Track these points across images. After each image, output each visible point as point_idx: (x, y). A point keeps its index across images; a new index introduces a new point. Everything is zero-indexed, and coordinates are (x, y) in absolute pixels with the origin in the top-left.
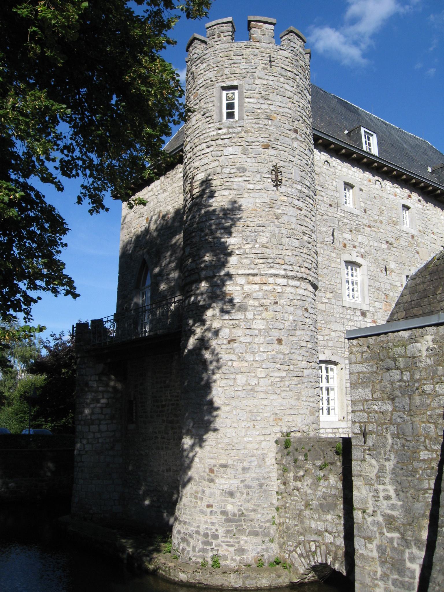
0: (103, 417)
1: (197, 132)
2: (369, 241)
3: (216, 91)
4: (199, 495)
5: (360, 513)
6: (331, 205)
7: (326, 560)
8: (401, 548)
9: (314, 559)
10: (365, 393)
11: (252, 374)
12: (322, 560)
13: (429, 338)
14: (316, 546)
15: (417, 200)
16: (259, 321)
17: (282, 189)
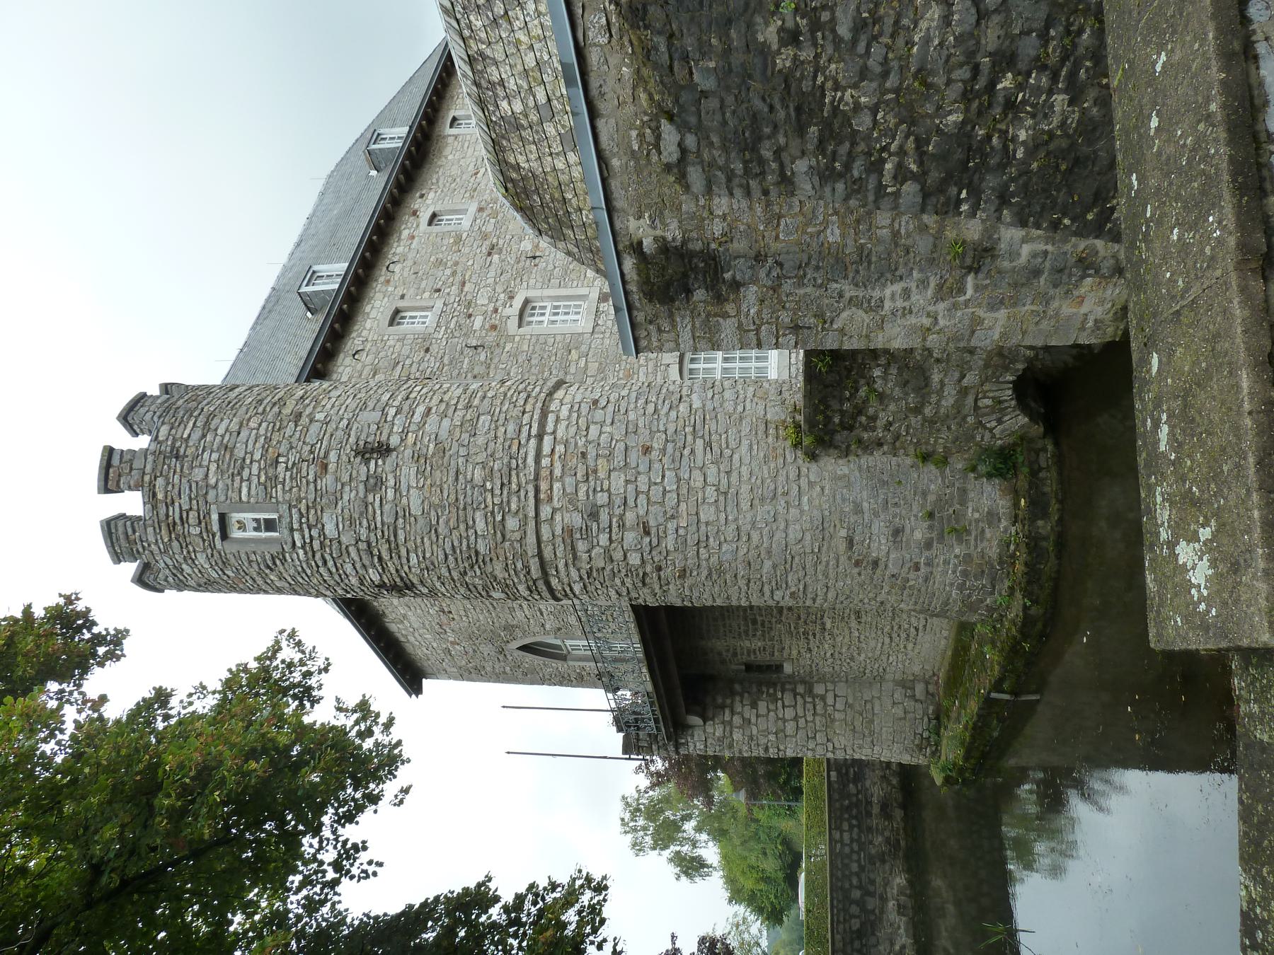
1: (301, 580)
2: (486, 286)
3: (230, 548)
6: (427, 350)
7: (1010, 383)
9: (1006, 401)
11: (700, 495)
13: (632, 224)
14: (984, 397)
15: (419, 200)
16: (613, 483)
17: (395, 441)
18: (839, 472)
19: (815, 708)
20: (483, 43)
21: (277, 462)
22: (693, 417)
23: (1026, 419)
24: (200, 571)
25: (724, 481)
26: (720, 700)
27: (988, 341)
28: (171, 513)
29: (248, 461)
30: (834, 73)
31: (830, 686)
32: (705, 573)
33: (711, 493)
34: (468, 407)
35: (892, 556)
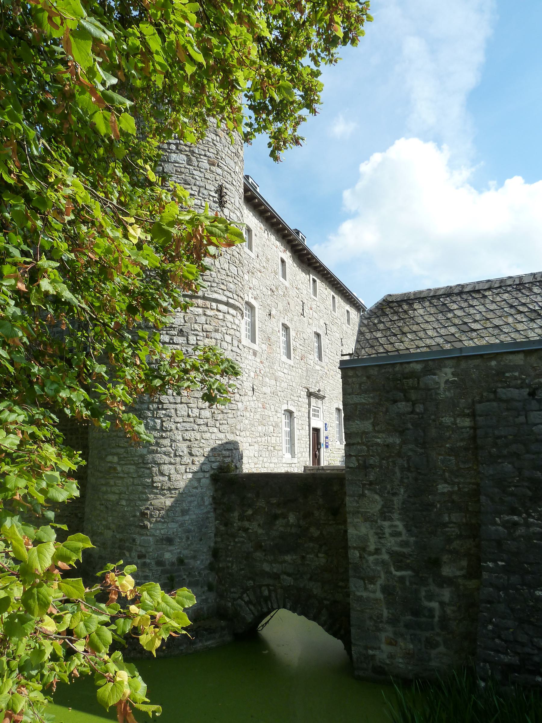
4: (127, 544)
9: (267, 605)
10: (367, 425)
13: (449, 371)
18: (206, 498)
21: (217, 135)
23: (250, 620)
25: (201, 422)
27: (354, 589)
33: (196, 412)
35: (151, 539)
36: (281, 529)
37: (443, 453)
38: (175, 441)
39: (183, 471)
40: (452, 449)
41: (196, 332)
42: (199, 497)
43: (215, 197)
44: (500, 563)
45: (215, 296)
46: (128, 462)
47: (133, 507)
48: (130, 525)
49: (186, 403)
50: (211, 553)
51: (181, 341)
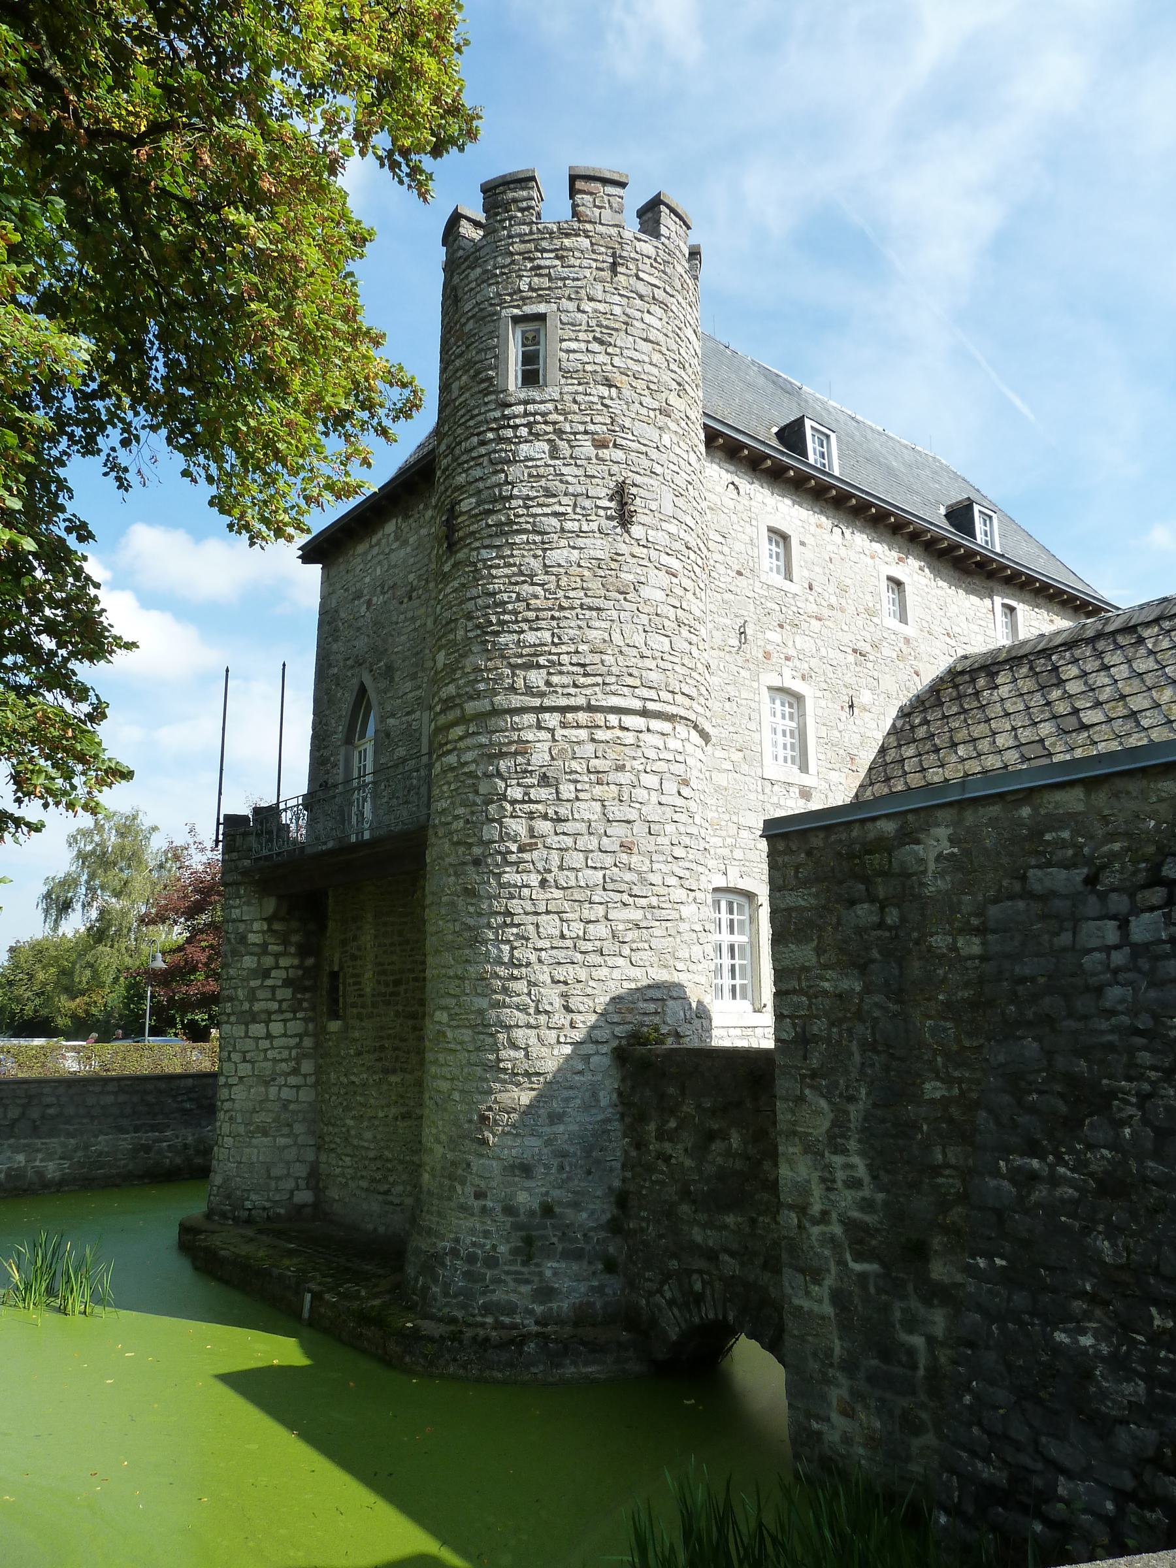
0: (275, 1006)
4: (460, 1172)
5: (793, 1215)
6: (739, 573)
7: (725, 1317)
8: (884, 1297)
9: (700, 1311)
12: (716, 1314)
13: (942, 832)
14: (703, 1281)
17: (637, 531)
18: (602, 1094)
19: (282, 1060)
20: (1155, 644)
21: (610, 386)
22: (670, 906)
23: (674, 1338)
24: (472, 289)
25: (589, 946)
26: (295, 938)
27: (790, 1291)
28: (545, 255)
29: (610, 350)
30: (1163, 1092)
31: (311, 1080)
32: (471, 922)
33: (577, 928)
34: (680, 623)
35: (494, 1163)
36: (719, 1161)
37: (933, 1012)
38: (535, 985)
39: (554, 1041)
40: (947, 1005)
41: (574, 776)
42: (587, 1090)
43: (610, 508)
44: (998, 1261)
45: (614, 701)
46: (461, 1023)
47: (467, 1104)
48: (464, 1137)
49: (557, 913)
50: (612, 1199)
51: (544, 796)
